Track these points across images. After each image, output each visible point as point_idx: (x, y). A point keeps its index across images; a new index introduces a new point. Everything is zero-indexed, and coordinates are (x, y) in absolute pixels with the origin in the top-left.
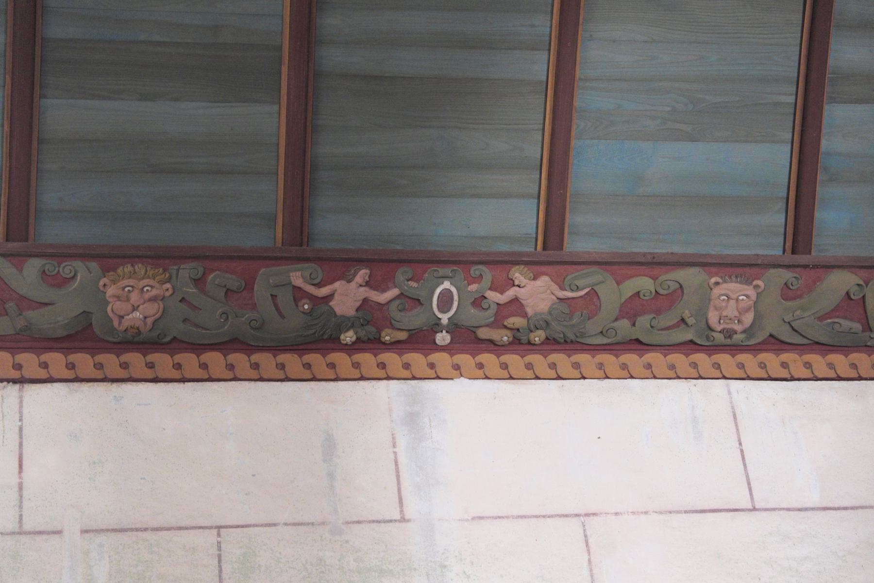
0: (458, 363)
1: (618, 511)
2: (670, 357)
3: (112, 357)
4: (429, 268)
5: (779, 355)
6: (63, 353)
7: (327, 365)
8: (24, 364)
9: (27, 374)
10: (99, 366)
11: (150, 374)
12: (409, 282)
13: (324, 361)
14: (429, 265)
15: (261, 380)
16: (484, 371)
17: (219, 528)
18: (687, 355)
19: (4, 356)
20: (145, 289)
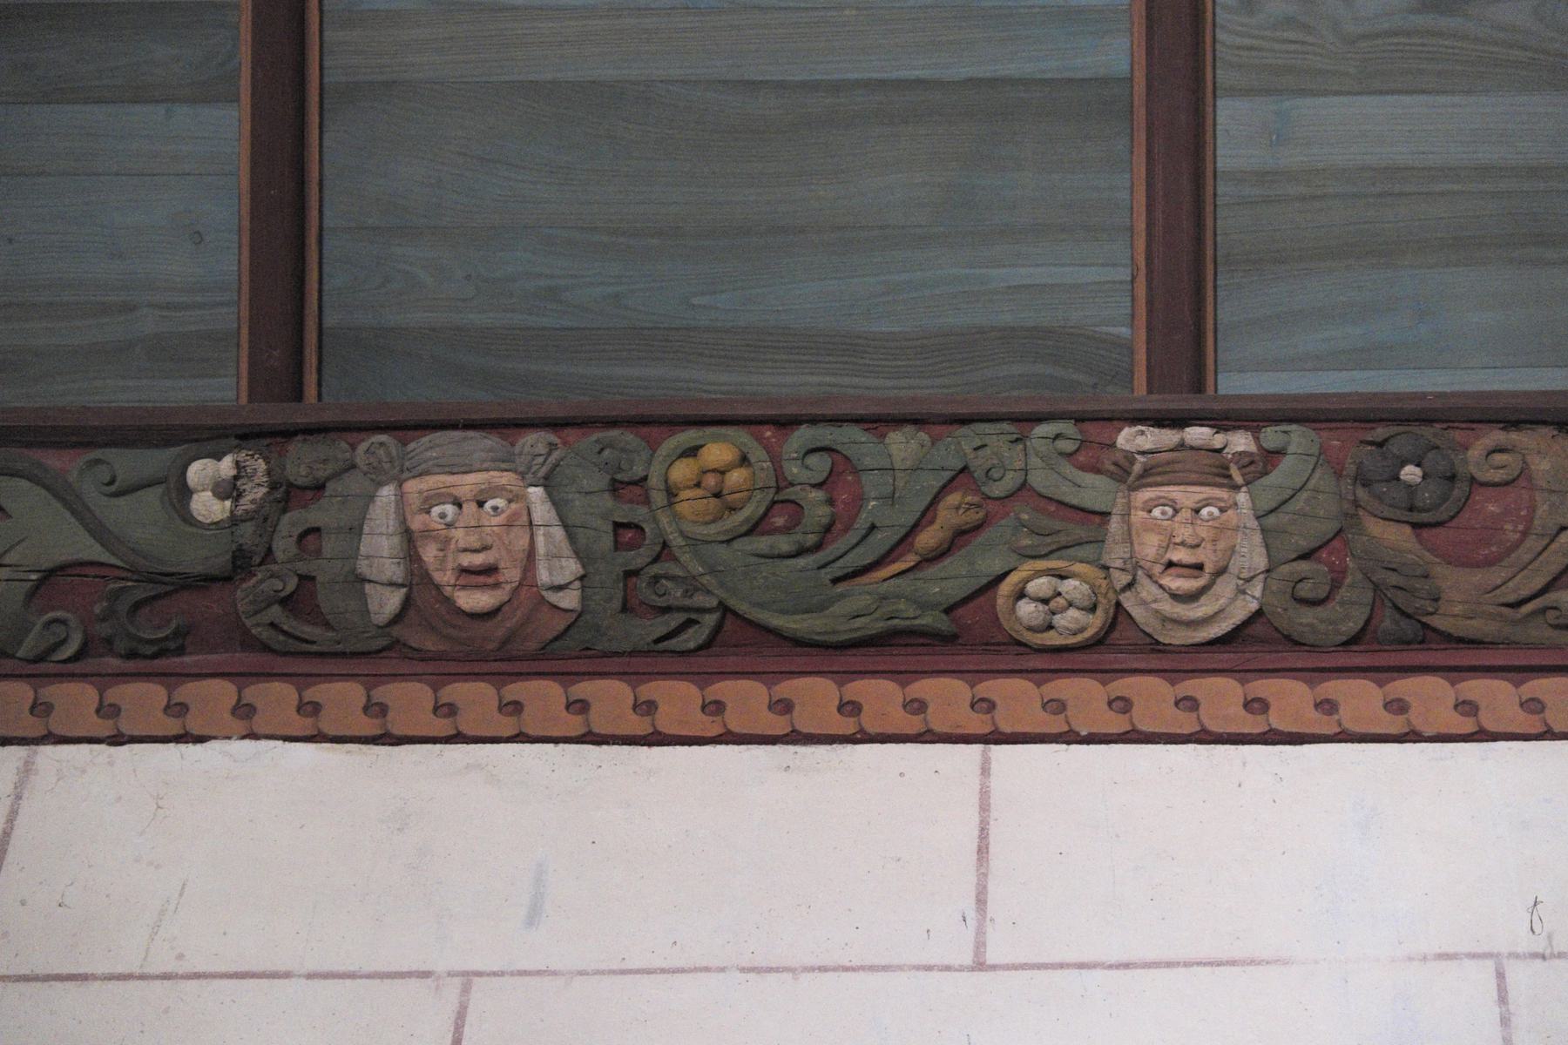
0: (296, 713)
1: (961, 919)
2: (1389, 687)
3: (887, 686)
4: (363, 440)
5: (1248, 681)
6: (629, 683)
7: (1044, 706)
8: (1548, 699)
9: (1277, 721)
10: (1467, 707)
11: (914, 724)
12: (981, 515)
13: (901, 695)
14: (363, 435)
15: (927, 737)
16: (1066, 716)
17: (980, 965)
18: (1517, 685)
19: (21, 692)
20: (1204, 512)
